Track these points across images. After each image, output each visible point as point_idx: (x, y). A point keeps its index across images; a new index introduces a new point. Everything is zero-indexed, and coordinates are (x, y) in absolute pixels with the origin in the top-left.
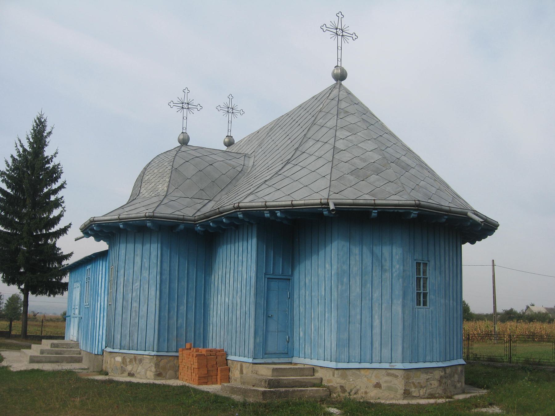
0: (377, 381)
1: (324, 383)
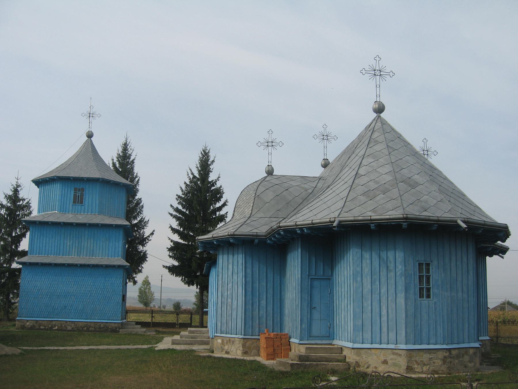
0: (385, 359)
1: (347, 360)
